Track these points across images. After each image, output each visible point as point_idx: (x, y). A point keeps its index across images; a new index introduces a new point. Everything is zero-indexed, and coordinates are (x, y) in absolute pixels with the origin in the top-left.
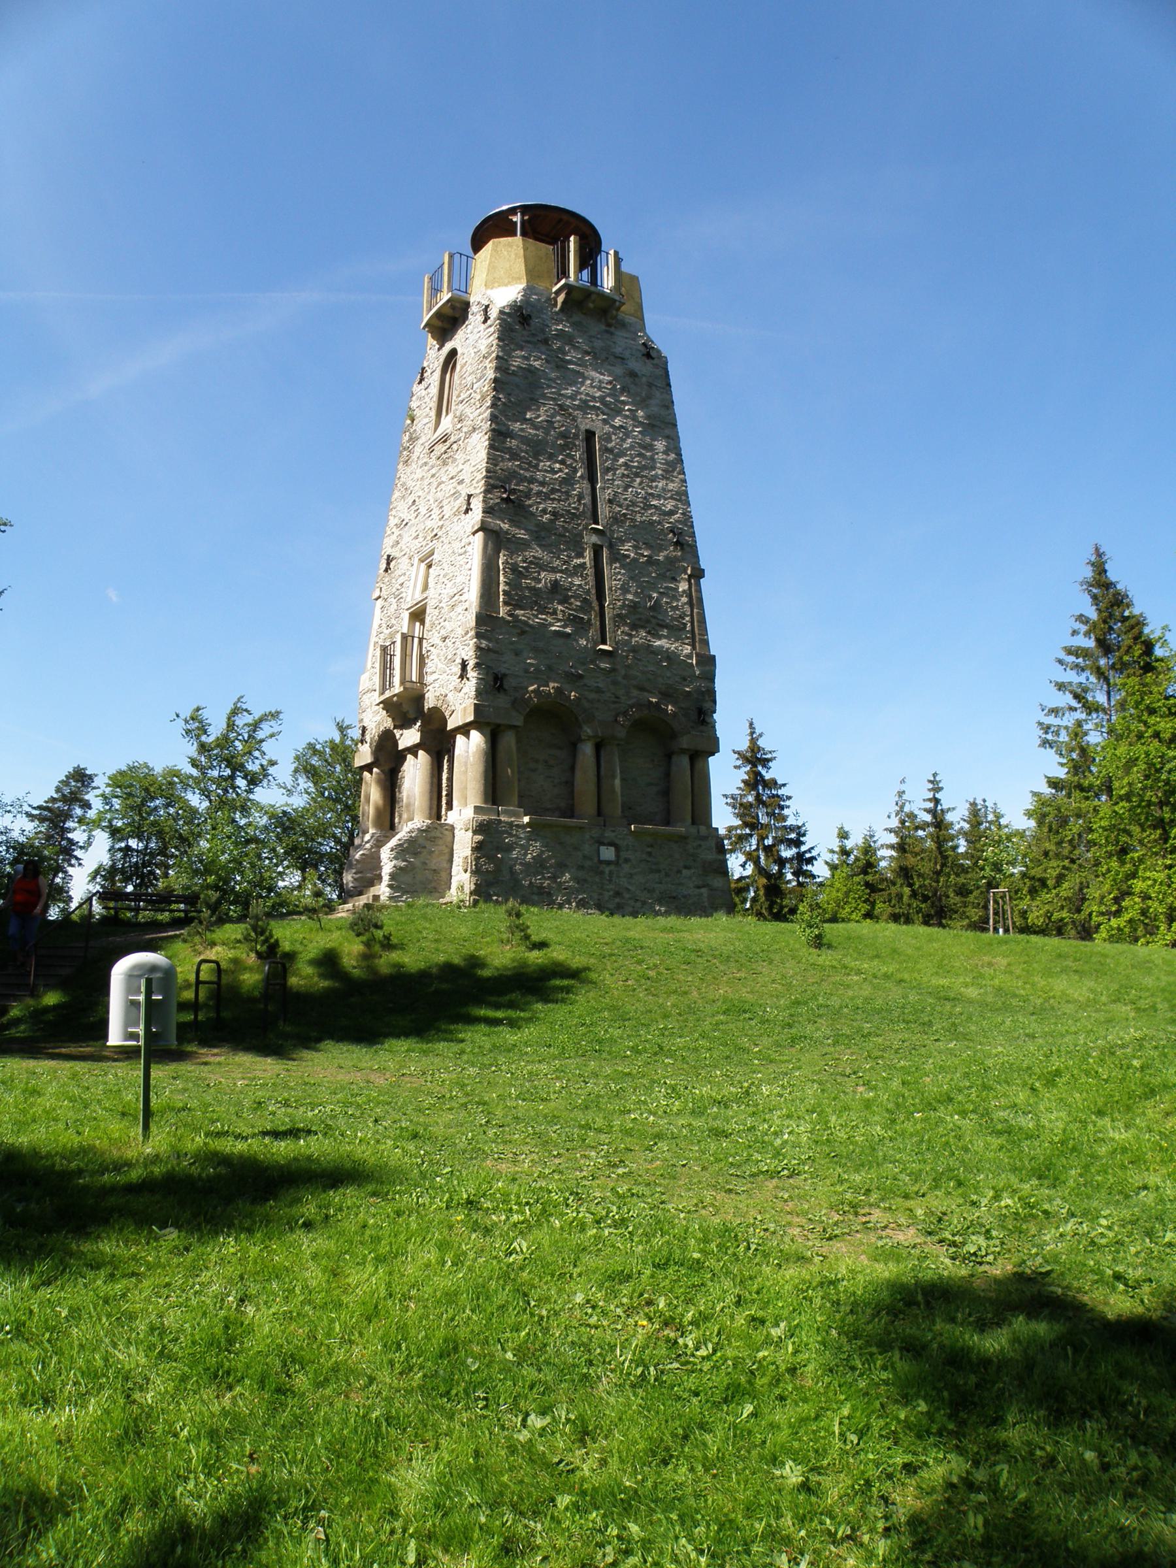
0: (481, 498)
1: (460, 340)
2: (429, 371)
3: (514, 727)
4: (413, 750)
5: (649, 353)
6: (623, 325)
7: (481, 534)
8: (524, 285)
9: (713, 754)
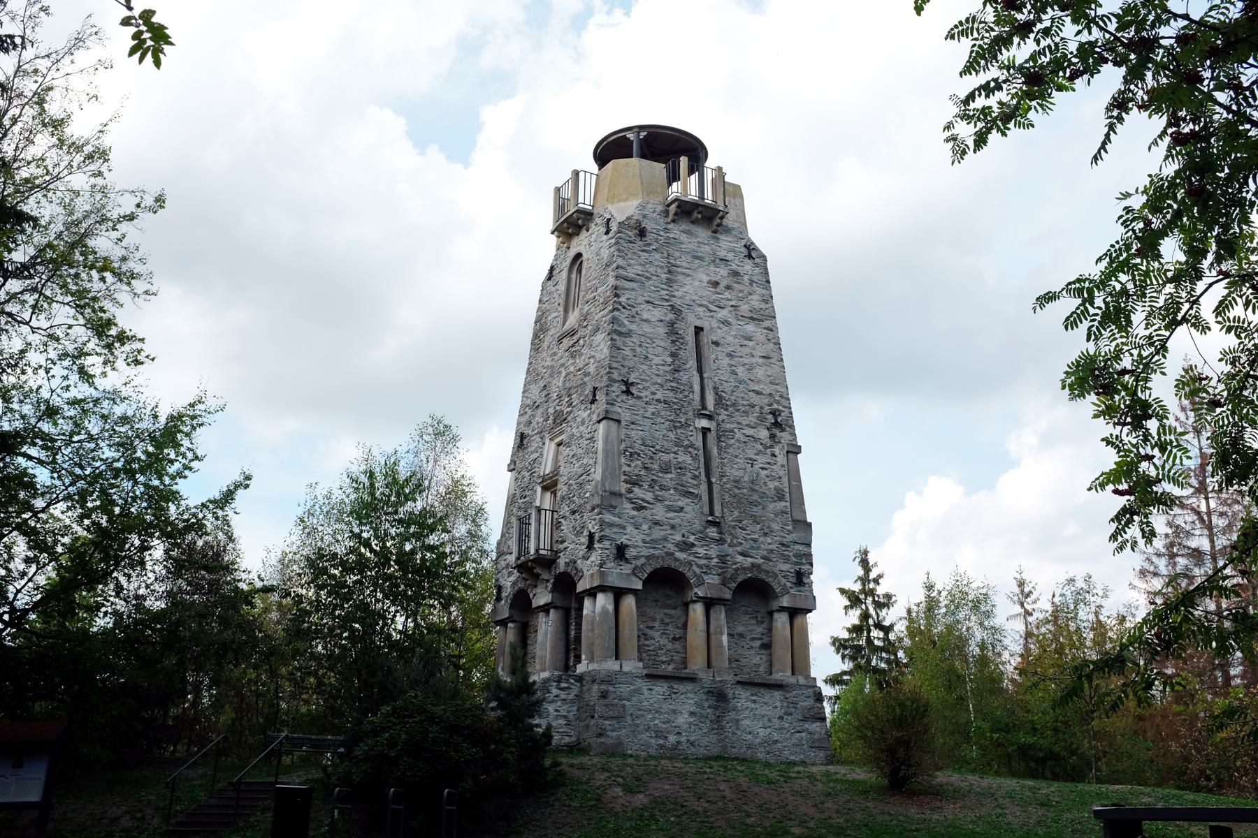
1: (581, 244)
4: (545, 609)
5: (751, 251)
6: (728, 230)
9: (810, 611)
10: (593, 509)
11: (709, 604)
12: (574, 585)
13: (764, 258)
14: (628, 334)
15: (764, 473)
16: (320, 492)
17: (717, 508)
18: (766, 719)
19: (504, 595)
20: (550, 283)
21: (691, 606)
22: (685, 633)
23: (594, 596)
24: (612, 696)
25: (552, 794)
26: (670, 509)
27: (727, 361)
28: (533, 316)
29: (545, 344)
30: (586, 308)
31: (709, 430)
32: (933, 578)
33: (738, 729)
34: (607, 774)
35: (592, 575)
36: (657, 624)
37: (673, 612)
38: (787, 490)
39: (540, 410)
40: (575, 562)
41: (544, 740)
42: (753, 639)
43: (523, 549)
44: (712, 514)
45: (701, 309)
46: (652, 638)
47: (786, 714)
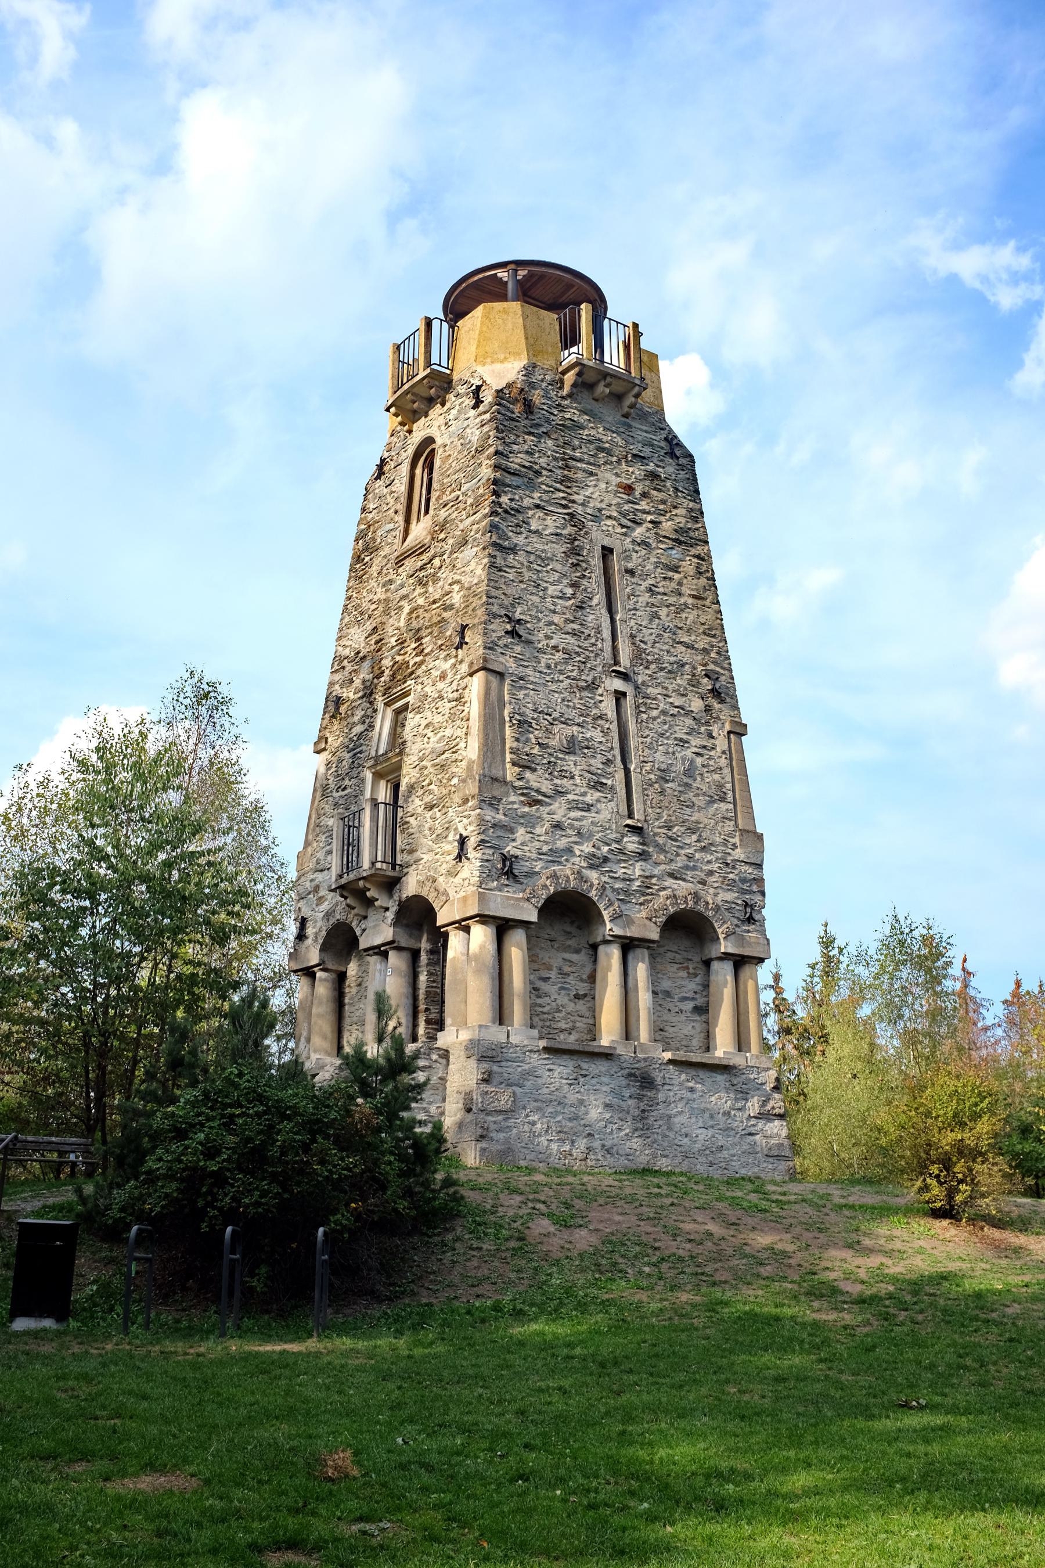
1: (433, 425)
2: (392, 464)
4: (381, 952)
7: (481, 674)
8: (524, 362)
9: (762, 960)
10: (466, 801)
11: (628, 946)
13: (690, 457)
14: (513, 550)
15: (699, 760)
16: (33, 777)
17: (637, 806)
18: (707, 1115)
19: (310, 931)
20: (379, 483)
21: (602, 949)
22: (593, 989)
23: (467, 930)
24: (496, 1079)
25: (446, 1230)
26: (574, 806)
27: (646, 598)
29: (374, 570)
30: (443, 513)
31: (624, 694)
32: (832, 930)
33: (670, 1129)
34: (519, 1198)
35: (465, 899)
37: (574, 957)
38: (729, 786)
39: (367, 664)
41: (434, 1145)
42: (684, 999)
43: (349, 864)
44: (630, 815)
45: (609, 522)
46: (547, 995)
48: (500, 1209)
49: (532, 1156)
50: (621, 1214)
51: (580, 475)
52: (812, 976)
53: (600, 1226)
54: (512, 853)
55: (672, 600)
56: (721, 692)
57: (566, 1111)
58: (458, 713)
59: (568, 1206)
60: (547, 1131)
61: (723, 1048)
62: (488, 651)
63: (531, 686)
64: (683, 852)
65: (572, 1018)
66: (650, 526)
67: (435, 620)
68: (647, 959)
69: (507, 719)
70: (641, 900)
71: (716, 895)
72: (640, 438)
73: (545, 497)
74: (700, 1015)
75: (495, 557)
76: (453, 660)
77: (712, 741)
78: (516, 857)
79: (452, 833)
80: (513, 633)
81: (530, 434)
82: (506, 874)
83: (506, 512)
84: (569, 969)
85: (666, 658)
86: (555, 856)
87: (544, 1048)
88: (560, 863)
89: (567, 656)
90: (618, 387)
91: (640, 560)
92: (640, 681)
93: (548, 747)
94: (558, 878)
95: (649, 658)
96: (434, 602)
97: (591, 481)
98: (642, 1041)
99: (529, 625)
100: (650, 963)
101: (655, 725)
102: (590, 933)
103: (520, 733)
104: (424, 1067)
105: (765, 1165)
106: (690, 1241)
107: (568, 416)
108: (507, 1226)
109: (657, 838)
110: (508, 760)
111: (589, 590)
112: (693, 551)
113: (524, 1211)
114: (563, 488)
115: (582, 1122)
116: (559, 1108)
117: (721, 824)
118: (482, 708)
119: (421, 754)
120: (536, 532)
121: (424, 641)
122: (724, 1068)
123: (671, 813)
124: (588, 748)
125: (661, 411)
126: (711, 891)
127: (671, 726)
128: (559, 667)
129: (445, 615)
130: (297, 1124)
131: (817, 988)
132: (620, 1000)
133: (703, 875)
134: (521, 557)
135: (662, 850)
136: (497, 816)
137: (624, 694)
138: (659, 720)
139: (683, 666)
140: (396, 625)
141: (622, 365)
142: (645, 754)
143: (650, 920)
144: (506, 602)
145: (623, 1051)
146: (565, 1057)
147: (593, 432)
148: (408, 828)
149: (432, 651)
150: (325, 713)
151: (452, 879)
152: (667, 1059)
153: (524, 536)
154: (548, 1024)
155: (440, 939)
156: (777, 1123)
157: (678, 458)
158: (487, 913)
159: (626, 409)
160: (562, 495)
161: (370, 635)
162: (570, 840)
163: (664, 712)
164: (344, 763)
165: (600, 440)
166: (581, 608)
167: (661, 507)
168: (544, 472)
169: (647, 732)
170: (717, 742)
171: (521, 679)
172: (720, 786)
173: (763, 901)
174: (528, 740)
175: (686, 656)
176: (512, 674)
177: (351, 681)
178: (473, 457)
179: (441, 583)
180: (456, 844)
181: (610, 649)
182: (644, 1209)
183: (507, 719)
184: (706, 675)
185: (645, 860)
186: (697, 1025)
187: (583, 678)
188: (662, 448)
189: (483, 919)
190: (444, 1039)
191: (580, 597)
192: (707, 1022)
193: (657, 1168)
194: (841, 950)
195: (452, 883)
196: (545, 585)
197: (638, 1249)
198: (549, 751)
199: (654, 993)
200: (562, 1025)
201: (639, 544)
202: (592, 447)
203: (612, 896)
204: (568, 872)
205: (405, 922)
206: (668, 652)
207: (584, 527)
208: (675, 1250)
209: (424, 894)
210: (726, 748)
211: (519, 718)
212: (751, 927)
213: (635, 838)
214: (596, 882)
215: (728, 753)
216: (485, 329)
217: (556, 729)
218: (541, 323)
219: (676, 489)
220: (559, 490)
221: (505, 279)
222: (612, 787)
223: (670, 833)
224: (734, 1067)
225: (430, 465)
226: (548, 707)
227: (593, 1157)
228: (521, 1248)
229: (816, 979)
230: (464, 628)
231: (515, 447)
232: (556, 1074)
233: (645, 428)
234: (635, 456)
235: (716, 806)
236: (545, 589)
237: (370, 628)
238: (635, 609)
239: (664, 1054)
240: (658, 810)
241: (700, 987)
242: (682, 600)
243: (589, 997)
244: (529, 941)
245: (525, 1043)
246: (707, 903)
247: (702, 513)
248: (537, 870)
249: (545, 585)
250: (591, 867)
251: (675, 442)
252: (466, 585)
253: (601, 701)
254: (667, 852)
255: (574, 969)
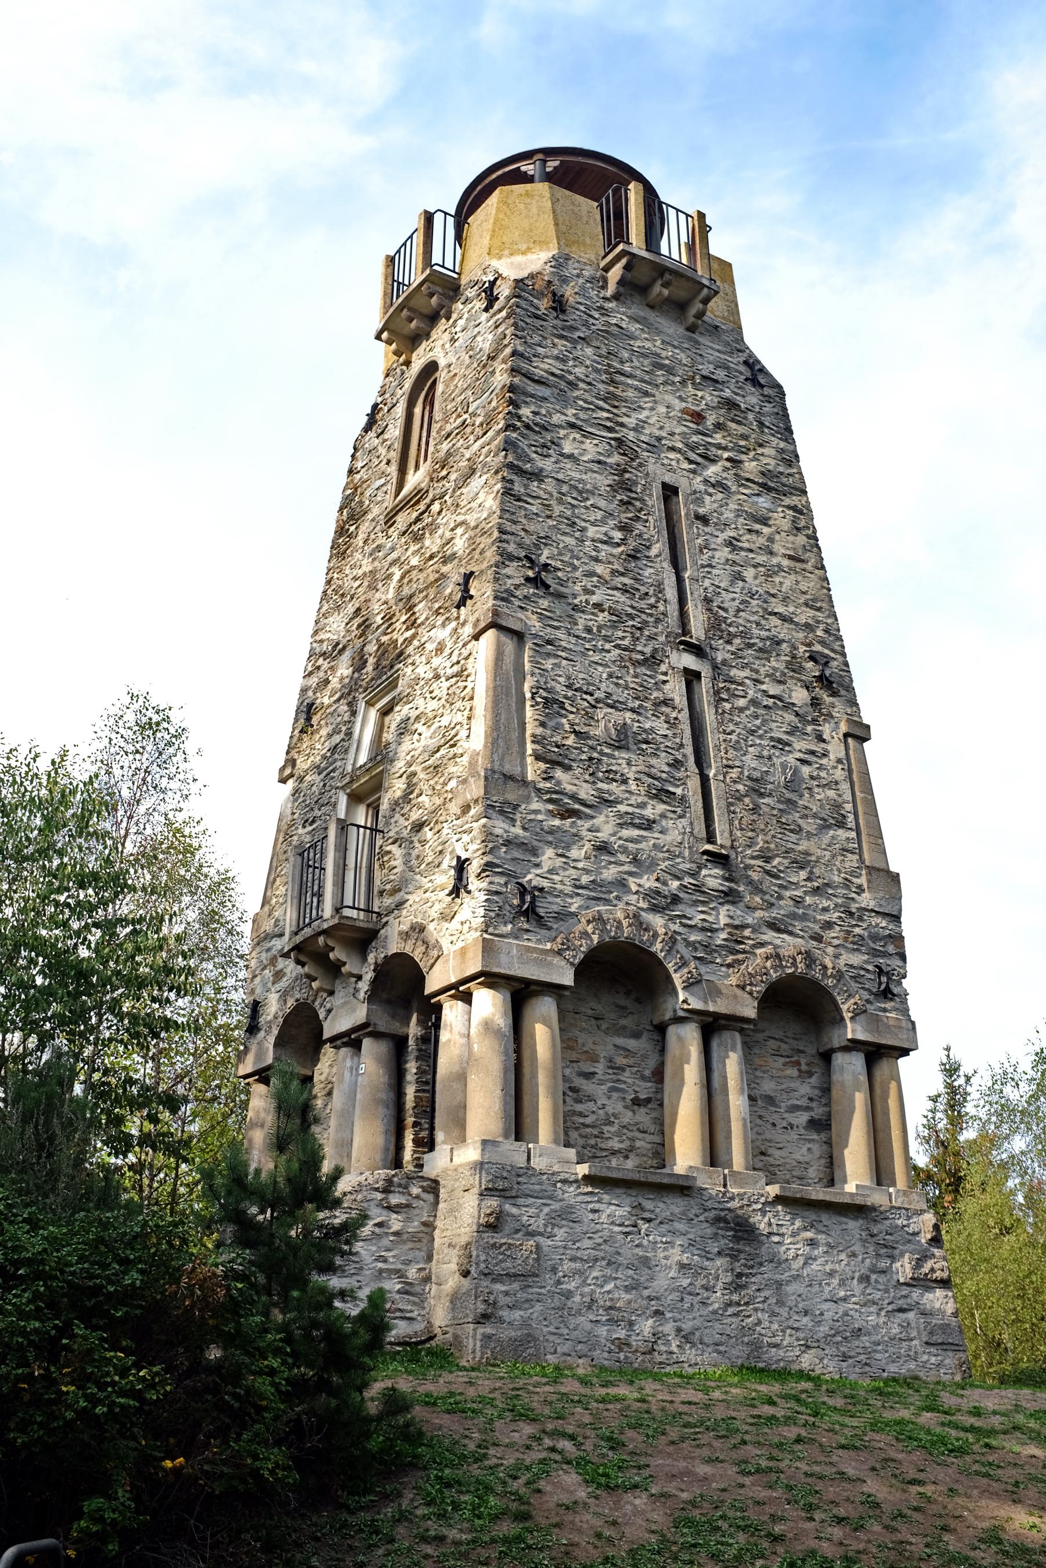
0: (490, 574)
1: (438, 347)
3: (555, 989)
4: (351, 1040)
5: (756, 373)
9: (905, 1052)
10: (466, 809)
11: (712, 1026)
12: (419, 978)
14: (537, 476)
15: (806, 770)
20: (372, 434)
21: (672, 1031)
22: (660, 1091)
23: (467, 998)
24: (509, 1226)
26: (627, 821)
27: (724, 553)
28: (337, 500)
29: (359, 540)
30: (445, 446)
31: (697, 675)
33: (780, 1303)
34: (528, 1429)
35: (463, 951)
36: (600, 1068)
37: (632, 1044)
38: (849, 807)
40: (422, 929)
44: (711, 838)
45: (672, 455)
46: (590, 1099)
47: (874, 1270)
48: (492, 1452)
49: (566, 1348)
50: (710, 1461)
51: (630, 394)
52: (933, 1111)
53: (671, 1488)
54: (534, 883)
55: (761, 559)
56: (833, 681)
57: (619, 1275)
58: (458, 691)
59: (615, 1444)
60: (589, 1308)
61: (855, 1178)
62: (499, 603)
63: (563, 654)
64: (788, 894)
65: (630, 1134)
66: (728, 464)
67: (432, 578)
68: (739, 1046)
69: (528, 695)
70: (730, 959)
71: (837, 956)
72: (711, 358)
73: (582, 415)
74: (819, 1132)
75: (511, 482)
76: (454, 624)
77: (823, 745)
78: (541, 890)
79: (448, 857)
80: (536, 581)
81: (561, 337)
82: (526, 914)
83: (527, 427)
84: (625, 1061)
85: (756, 632)
86: (599, 891)
87: (585, 1177)
88: (607, 902)
89: (615, 618)
90: (681, 292)
91: (715, 505)
92: (719, 659)
93: (589, 738)
94: (604, 923)
95: (731, 629)
96: (431, 557)
97: (646, 402)
98: (735, 1168)
99: (560, 574)
100: (745, 1056)
101: (743, 718)
102: (655, 1009)
103: (547, 715)
104: (399, 1206)
105: (925, 1357)
106: (840, 1520)
107: (614, 321)
108: (499, 1489)
109: (750, 873)
110: (529, 751)
111: (646, 536)
112: (787, 501)
113: (537, 1455)
114: (607, 407)
115: (646, 1293)
116: (608, 1272)
117: (840, 858)
118: (491, 676)
119: (409, 758)
120: (570, 456)
121: (416, 609)
122: (857, 1210)
123: (768, 838)
124: (647, 742)
125: (738, 328)
126: (830, 950)
127: (764, 721)
128: (603, 632)
129: (445, 569)
130: (36, 1296)
131: (941, 1126)
132: (701, 1110)
133: (817, 928)
134: (549, 485)
135: (757, 888)
136: (512, 829)
137: (697, 675)
138: (748, 712)
139: (779, 643)
140: (384, 598)
141: (684, 261)
142: (729, 756)
143: (743, 988)
144: (527, 541)
145: (710, 1183)
146: (618, 1191)
147: (648, 344)
148: (389, 861)
149: (427, 619)
150: (294, 729)
151: (446, 925)
152: (773, 1195)
153: (553, 460)
154: (592, 1142)
155: (432, 1014)
156: (939, 1293)
157: (762, 386)
158: (496, 970)
159: (691, 320)
160: (606, 415)
161: (351, 619)
162: (621, 869)
163: (754, 702)
164: (314, 788)
165: (658, 355)
166: (635, 558)
167: (742, 443)
168: (582, 385)
169: (732, 727)
170: (829, 748)
171: (549, 642)
172: (837, 806)
173: (904, 967)
174: (557, 728)
175: (783, 631)
176: (535, 636)
177: (327, 682)
178: (484, 366)
179: (440, 532)
180: (452, 872)
181: (676, 614)
182: (751, 1450)
183: (528, 695)
184: (812, 658)
185: (733, 903)
186: (815, 1147)
187: (639, 648)
188: (741, 373)
189: (490, 979)
190: (438, 1163)
191: (632, 543)
192: (829, 1143)
193: (761, 1365)
194: (968, 1079)
195: (451, 932)
196: (583, 524)
197: (742, 1538)
198: (590, 742)
199: (752, 1099)
200: (615, 1144)
201: (713, 486)
202: (646, 362)
203: (686, 953)
204: (620, 915)
205: (384, 996)
206: (758, 624)
207: (637, 457)
208: (812, 1544)
209: (408, 950)
210: (842, 754)
211: (545, 694)
212: (889, 1005)
213: (718, 871)
214: (661, 931)
215: (845, 760)
216: (501, 216)
217: (600, 714)
218: (576, 209)
219: (761, 424)
220: (602, 409)
221: (531, 173)
222: (683, 799)
223: (768, 867)
224: (873, 1209)
225: (429, 401)
226: (589, 684)
227: (663, 1348)
228: (519, 1539)
229: (939, 1115)
230: (468, 577)
231: (540, 350)
232: (604, 1218)
233: (717, 347)
234: (704, 378)
235: (831, 832)
236: (583, 530)
237: (353, 610)
238: (710, 566)
239: (768, 1188)
240: (750, 834)
241: (817, 1092)
242: (775, 561)
243: (655, 1104)
244: (561, 1020)
245: (556, 1168)
246: (825, 967)
247: (797, 456)
248: (573, 909)
249: (583, 524)
250: (654, 909)
251: (757, 367)
252: (473, 524)
253: (665, 682)
254: (765, 893)
255: (631, 1061)
